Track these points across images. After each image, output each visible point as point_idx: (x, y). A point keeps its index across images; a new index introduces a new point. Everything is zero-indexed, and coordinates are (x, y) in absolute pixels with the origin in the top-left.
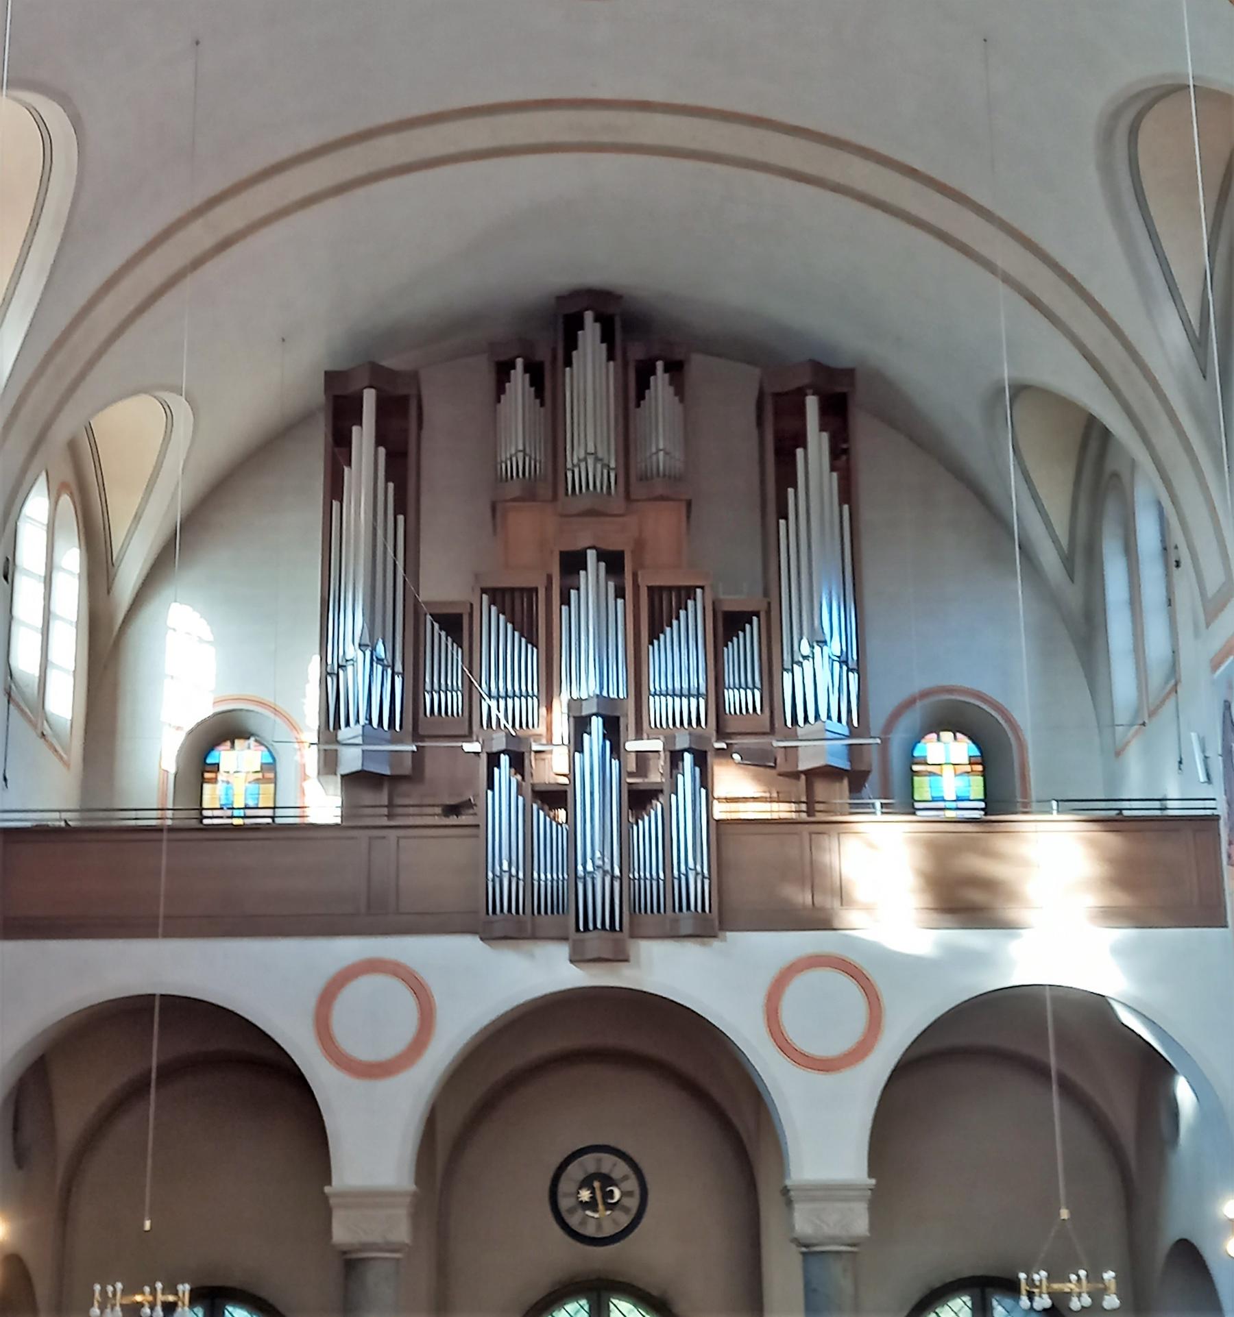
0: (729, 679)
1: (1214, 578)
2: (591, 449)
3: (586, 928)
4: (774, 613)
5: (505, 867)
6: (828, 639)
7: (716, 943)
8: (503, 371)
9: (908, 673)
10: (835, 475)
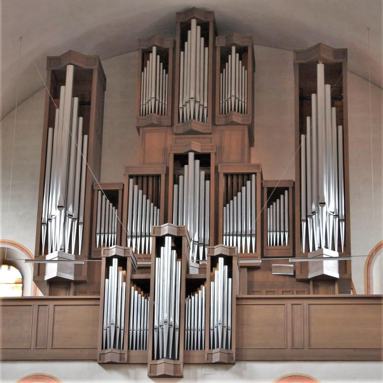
2: (192, 95)
6: (326, 201)
8: (145, 55)
10: (334, 109)
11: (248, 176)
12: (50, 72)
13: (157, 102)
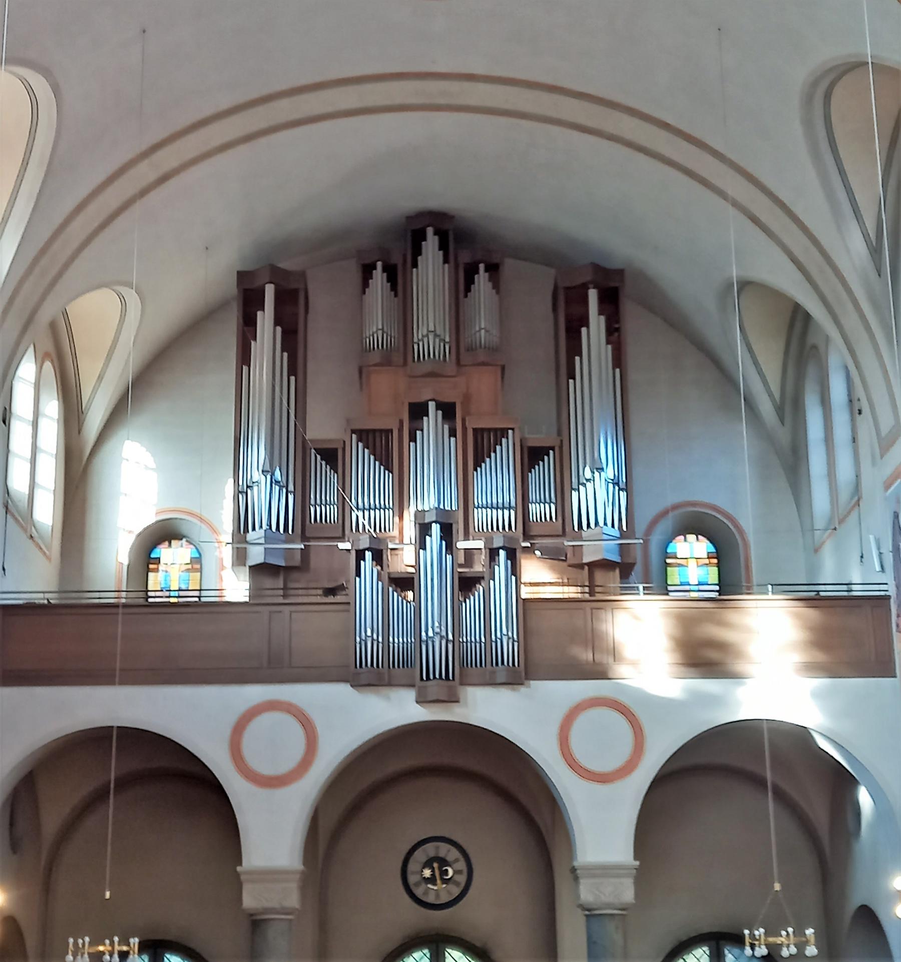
0: (532, 496)
1: (887, 422)
2: (431, 328)
3: (428, 678)
4: (565, 448)
5: (369, 633)
6: (605, 466)
7: (523, 689)
8: (367, 271)
9: (663, 492)
10: (610, 347)
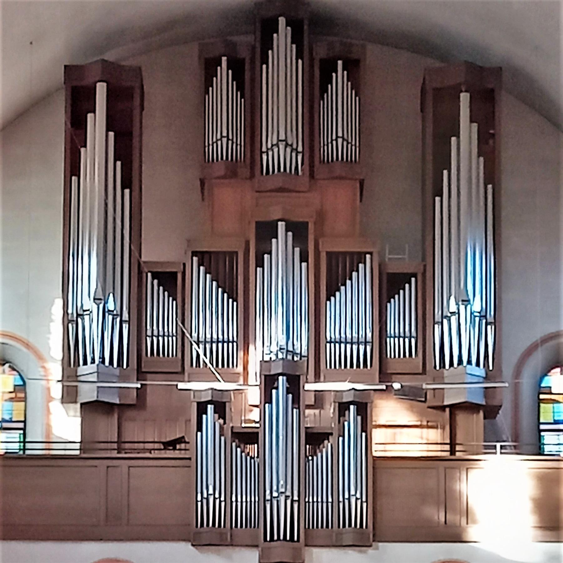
0: (391, 328)
3: (272, 539)
4: (429, 274)
5: (211, 491)
7: (370, 551)
8: (210, 68)
11: (360, 257)
12: (70, 89)
13: (230, 142)
